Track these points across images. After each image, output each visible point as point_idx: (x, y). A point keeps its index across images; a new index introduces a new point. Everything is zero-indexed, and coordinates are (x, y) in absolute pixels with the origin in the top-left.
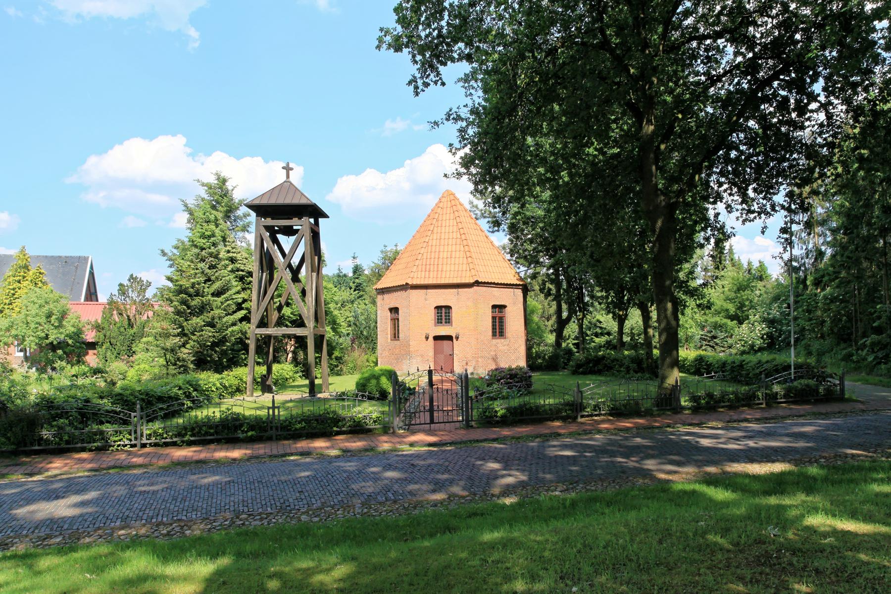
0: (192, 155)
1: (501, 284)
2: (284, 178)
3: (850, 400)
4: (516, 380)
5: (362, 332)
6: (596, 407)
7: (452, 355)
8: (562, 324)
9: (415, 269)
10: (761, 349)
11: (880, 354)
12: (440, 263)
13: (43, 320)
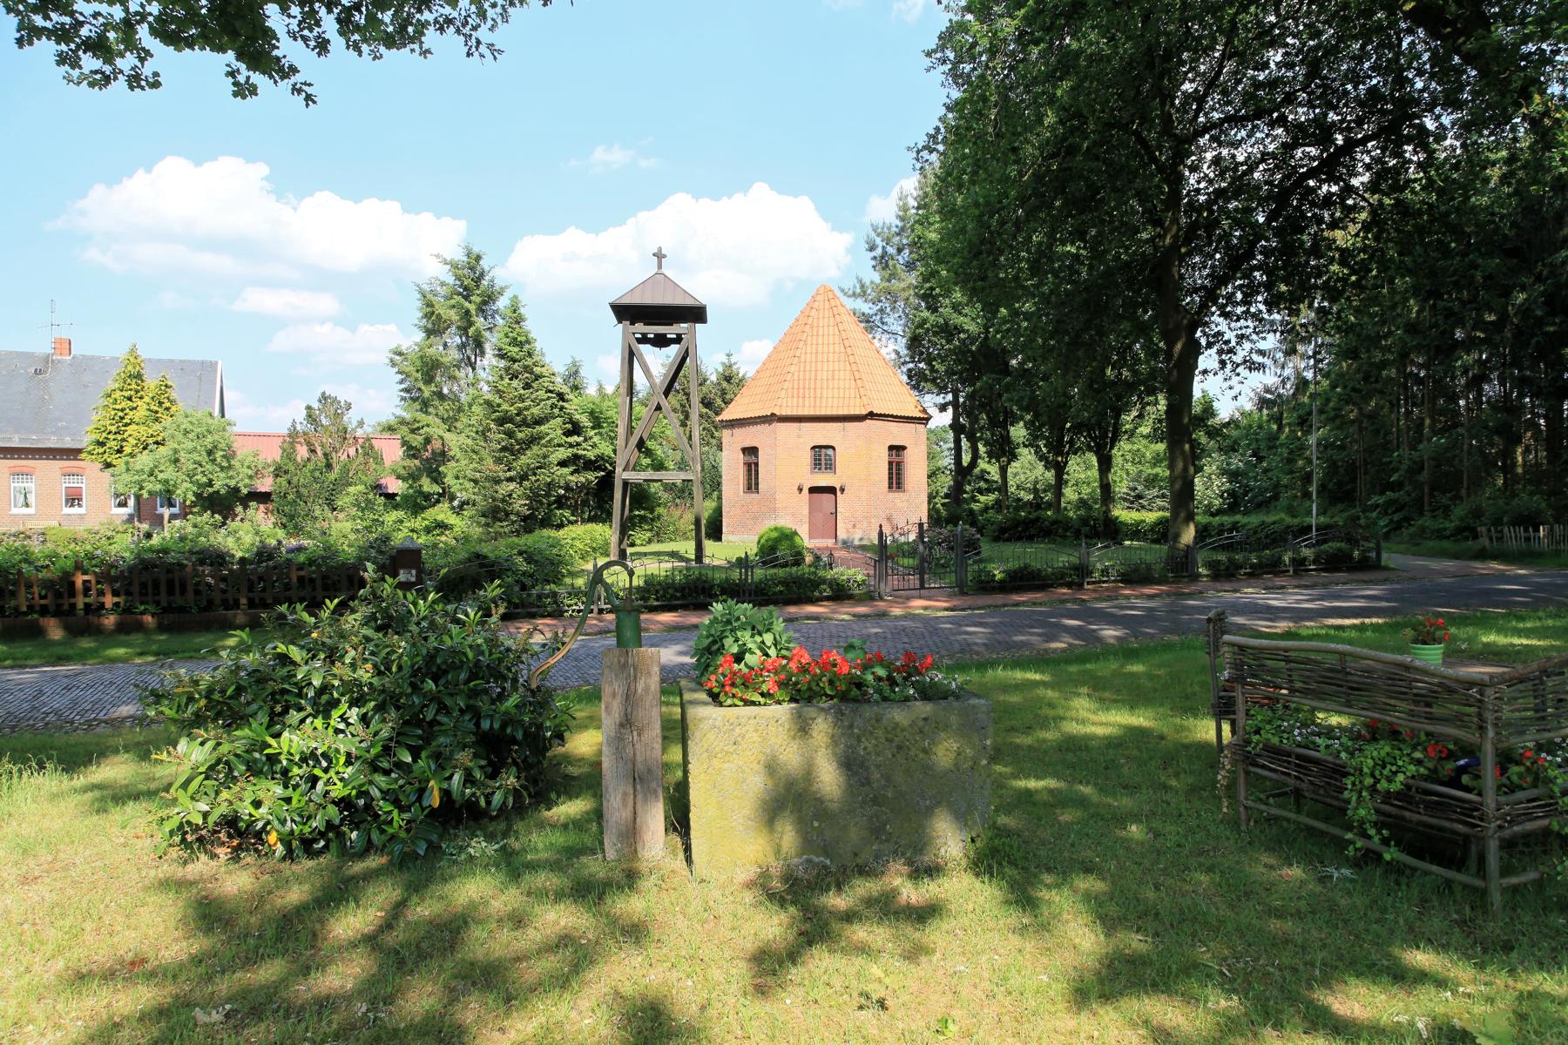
0: (279, 194)
3: (1386, 568)
6: (1105, 572)
9: (783, 394)
10: (1219, 512)
11: (1396, 517)
13: (204, 458)
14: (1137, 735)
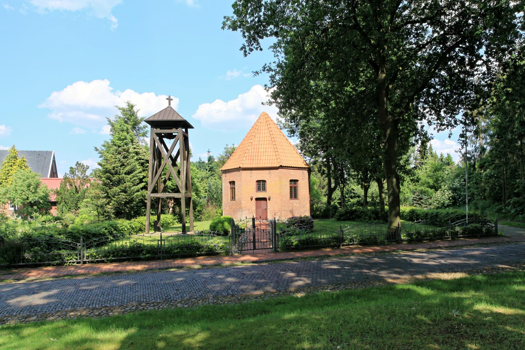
0: (113, 91)
1: (295, 167)
2: (167, 105)
3: (501, 236)
4: (304, 224)
5: (213, 196)
6: (351, 240)
7: (266, 209)
8: (331, 191)
9: (244, 158)
10: (448, 206)
11: (519, 209)
12: (259, 155)
13: (25, 189)
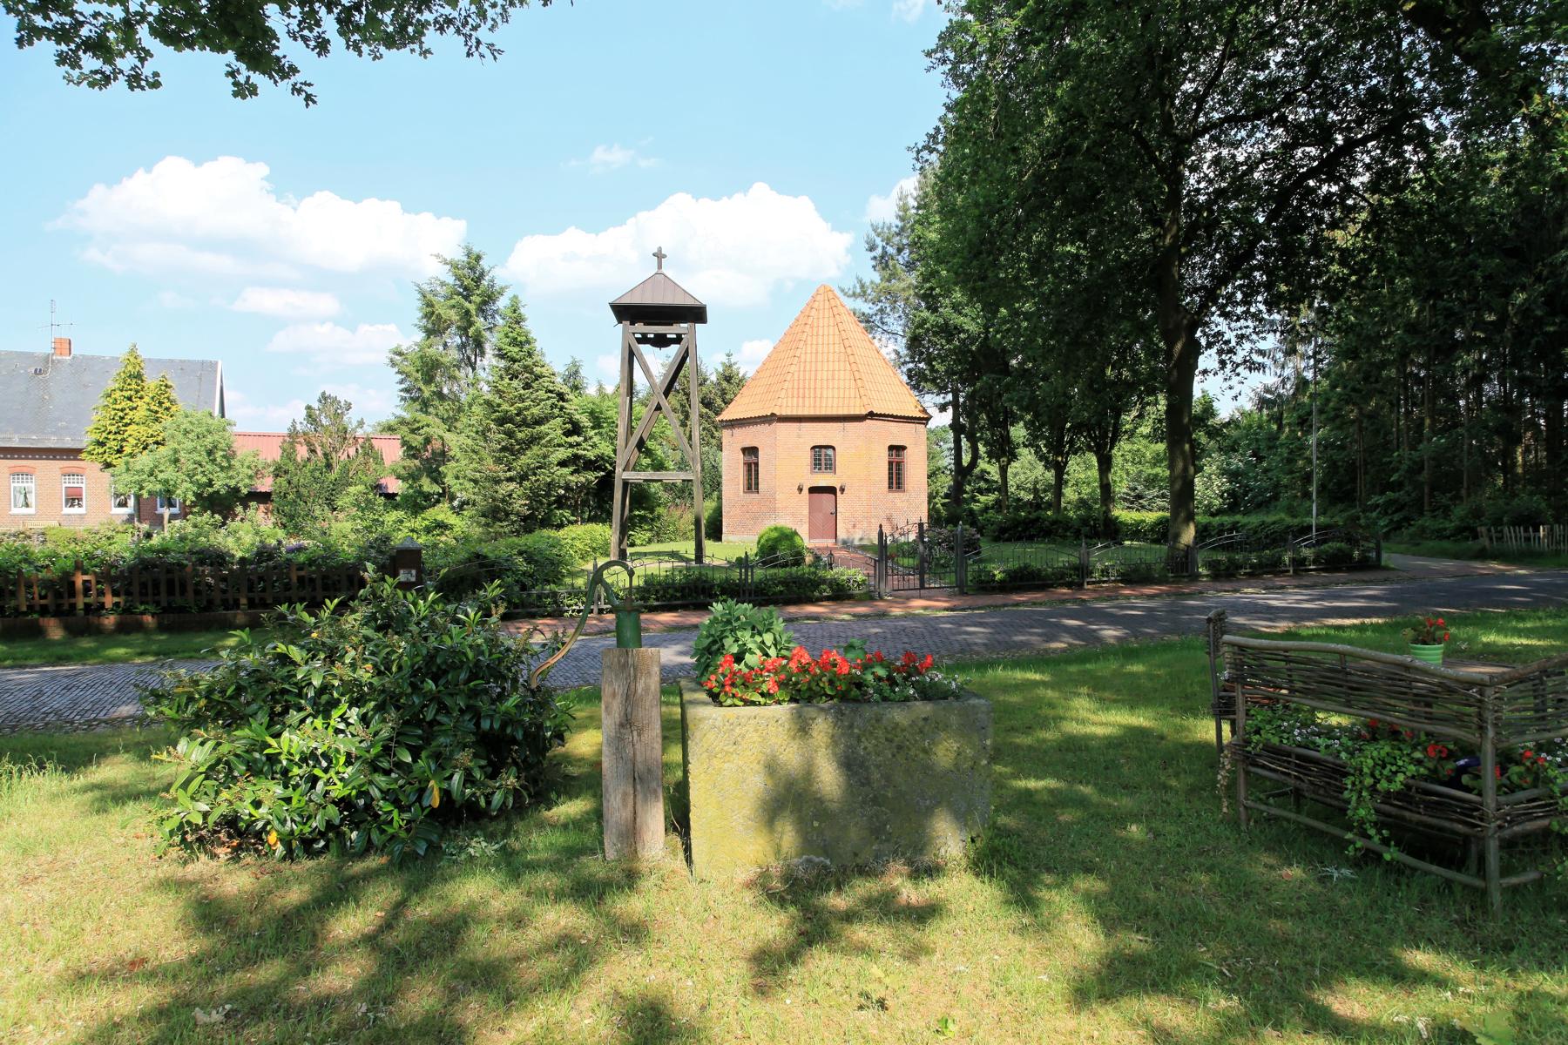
0: (279, 194)
3: (1386, 568)
6: (1105, 572)
9: (783, 394)
10: (1219, 512)
11: (1396, 517)
13: (204, 458)
14: (1137, 735)
